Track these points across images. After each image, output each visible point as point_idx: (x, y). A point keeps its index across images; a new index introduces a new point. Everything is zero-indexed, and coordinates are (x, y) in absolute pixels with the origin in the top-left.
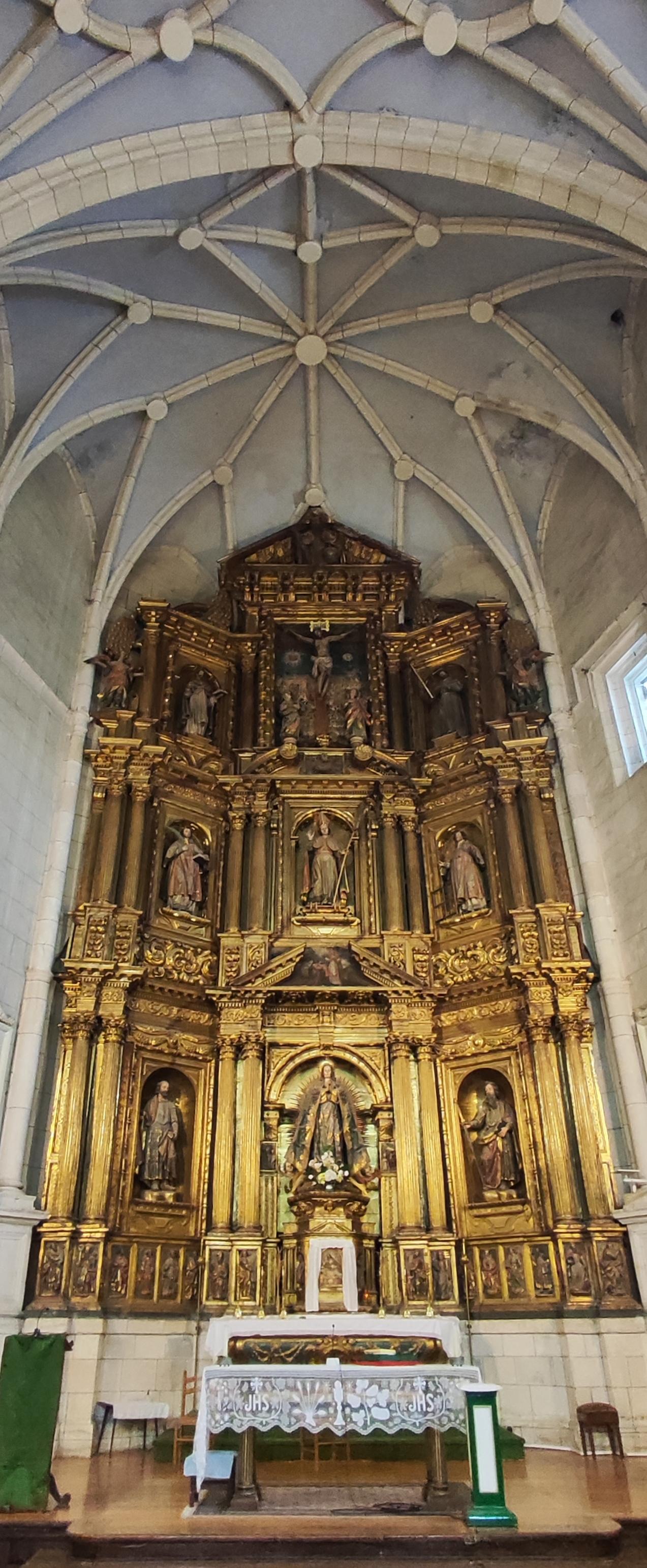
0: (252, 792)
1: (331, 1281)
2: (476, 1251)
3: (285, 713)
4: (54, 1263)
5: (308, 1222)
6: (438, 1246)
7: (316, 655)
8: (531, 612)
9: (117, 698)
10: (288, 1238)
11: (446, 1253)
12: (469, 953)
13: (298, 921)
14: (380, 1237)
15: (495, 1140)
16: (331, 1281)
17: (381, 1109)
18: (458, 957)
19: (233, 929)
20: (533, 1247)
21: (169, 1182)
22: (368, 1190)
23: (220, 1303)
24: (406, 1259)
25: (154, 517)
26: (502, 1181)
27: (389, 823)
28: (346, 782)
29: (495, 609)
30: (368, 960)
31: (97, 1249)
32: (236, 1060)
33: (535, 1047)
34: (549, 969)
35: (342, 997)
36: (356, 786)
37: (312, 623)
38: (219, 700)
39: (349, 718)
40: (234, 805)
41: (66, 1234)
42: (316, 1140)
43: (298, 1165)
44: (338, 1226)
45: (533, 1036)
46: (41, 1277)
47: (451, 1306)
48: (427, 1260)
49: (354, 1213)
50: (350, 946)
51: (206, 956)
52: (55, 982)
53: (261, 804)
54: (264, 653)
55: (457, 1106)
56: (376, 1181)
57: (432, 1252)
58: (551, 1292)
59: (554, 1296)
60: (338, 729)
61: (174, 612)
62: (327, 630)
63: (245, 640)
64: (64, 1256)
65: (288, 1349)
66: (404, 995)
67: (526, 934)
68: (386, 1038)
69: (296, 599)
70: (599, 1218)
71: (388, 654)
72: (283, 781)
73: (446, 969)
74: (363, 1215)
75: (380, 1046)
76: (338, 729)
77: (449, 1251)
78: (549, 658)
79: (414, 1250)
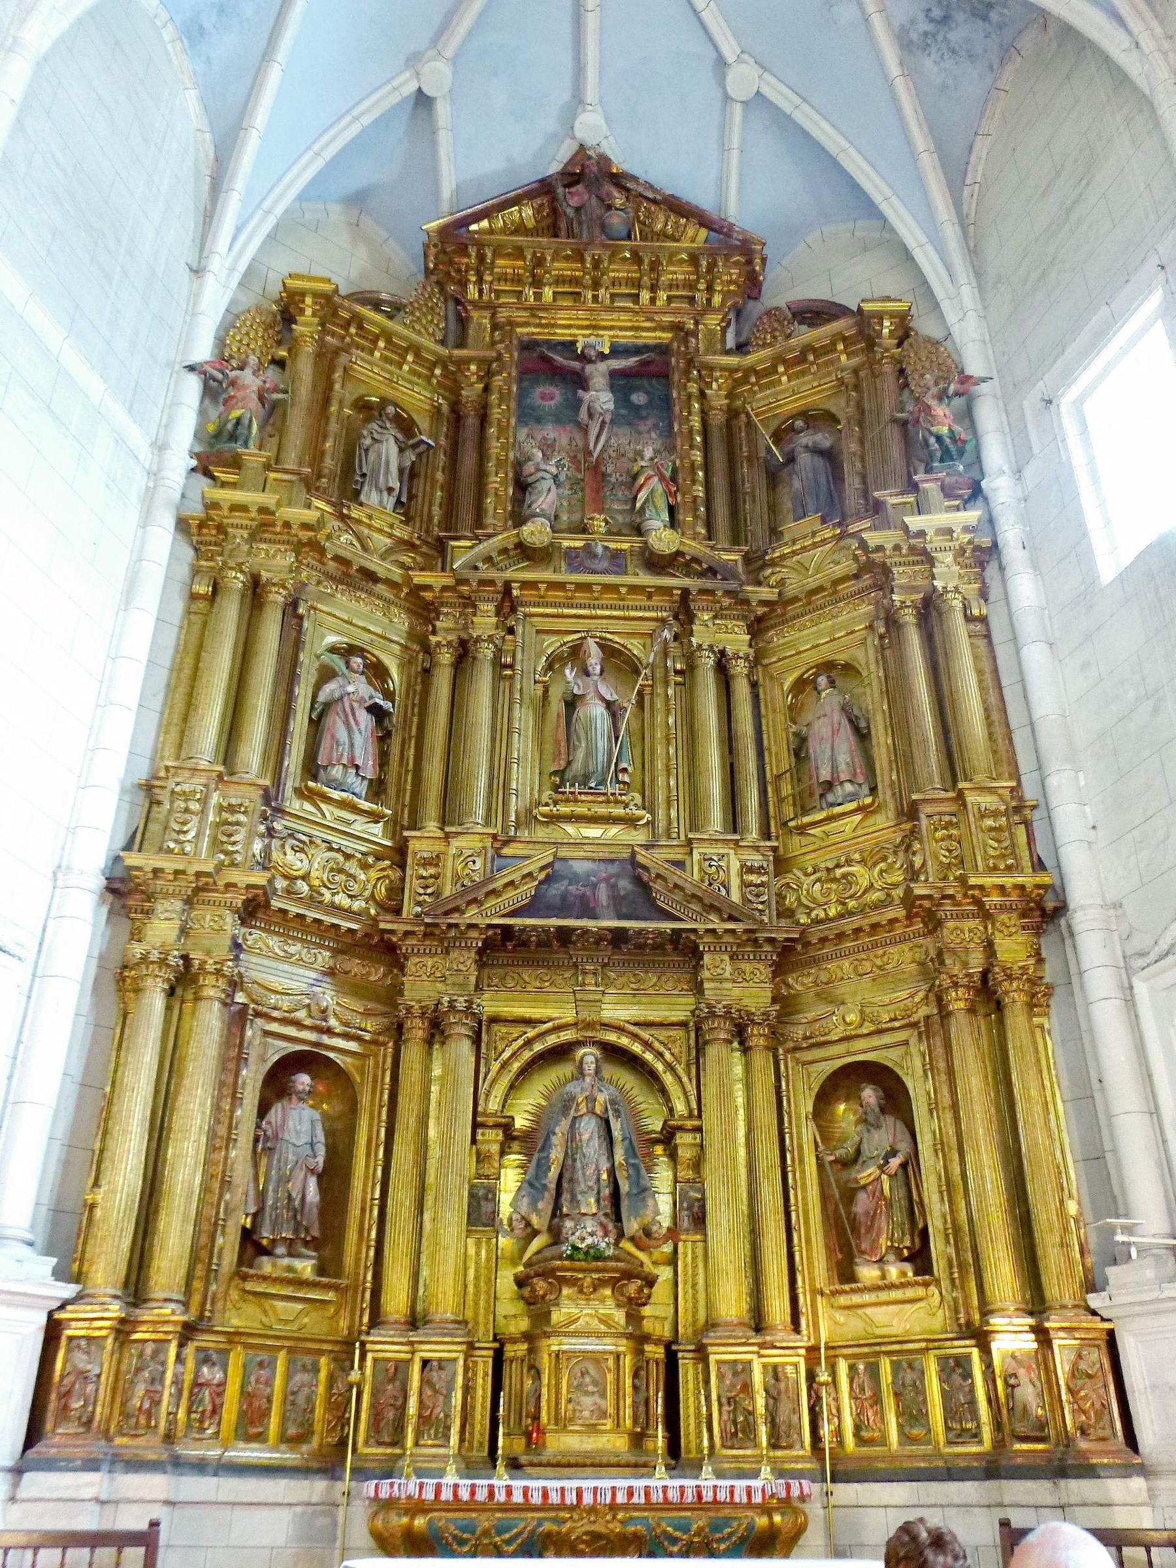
0: (469, 603)
1: (586, 1414)
2: (843, 1367)
3: (530, 480)
4: (83, 1376)
5: (549, 1313)
6: (775, 1357)
7: (586, 388)
8: (951, 318)
9: (242, 430)
10: (514, 1341)
11: (789, 1369)
12: (839, 872)
13: (544, 816)
14: (675, 1341)
15: (878, 1178)
16: (586, 1414)
17: (681, 1128)
18: (818, 880)
19: (432, 827)
20: (942, 1360)
21: (306, 1244)
22: (655, 1263)
23: (389, 1451)
24: (720, 1377)
25: (314, 142)
26: (888, 1248)
27: (708, 661)
28: (634, 589)
29: (892, 315)
30: (665, 879)
31: (166, 1352)
32: (429, 1042)
33: (953, 1020)
34: (981, 888)
35: (618, 938)
36: (650, 597)
37: (580, 339)
38: (419, 455)
39: (639, 490)
40: (438, 624)
41: (107, 1323)
42: (567, 1175)
43: (535, 1220)
44: (601, 1321)
45: (947, 1005)
46: (59, 1398)
47: (797, 1459)
48: (758, 1378)
49: (630, 1299)
50: (634, 854)
51: (383, 870)
52: (110, 897)
53: (485, 621)
54: (498, 381)
55: (811, 1124)
56: (667, 1248)
57: (764, 1366)
58: (975, 1436)
59: (981, 1442)
60: (621, 512)
61: (346, 303)
62: (607, 351)
63: (467, 361)
64: (102, 1365)
65: (508, 1530)
66: (728, 938)
67: (939, 834)
68: (693, 1012)
69: (554, 300)
70: (1063, 1307)
71: (708, 392)
72: (525, 585)
73: (798, 899)
74: (644, 1304)
75: (683, 1024)
76: (621, 512)
77: (796, 1365)
78: (984, 388)
79: (735, 1361)
